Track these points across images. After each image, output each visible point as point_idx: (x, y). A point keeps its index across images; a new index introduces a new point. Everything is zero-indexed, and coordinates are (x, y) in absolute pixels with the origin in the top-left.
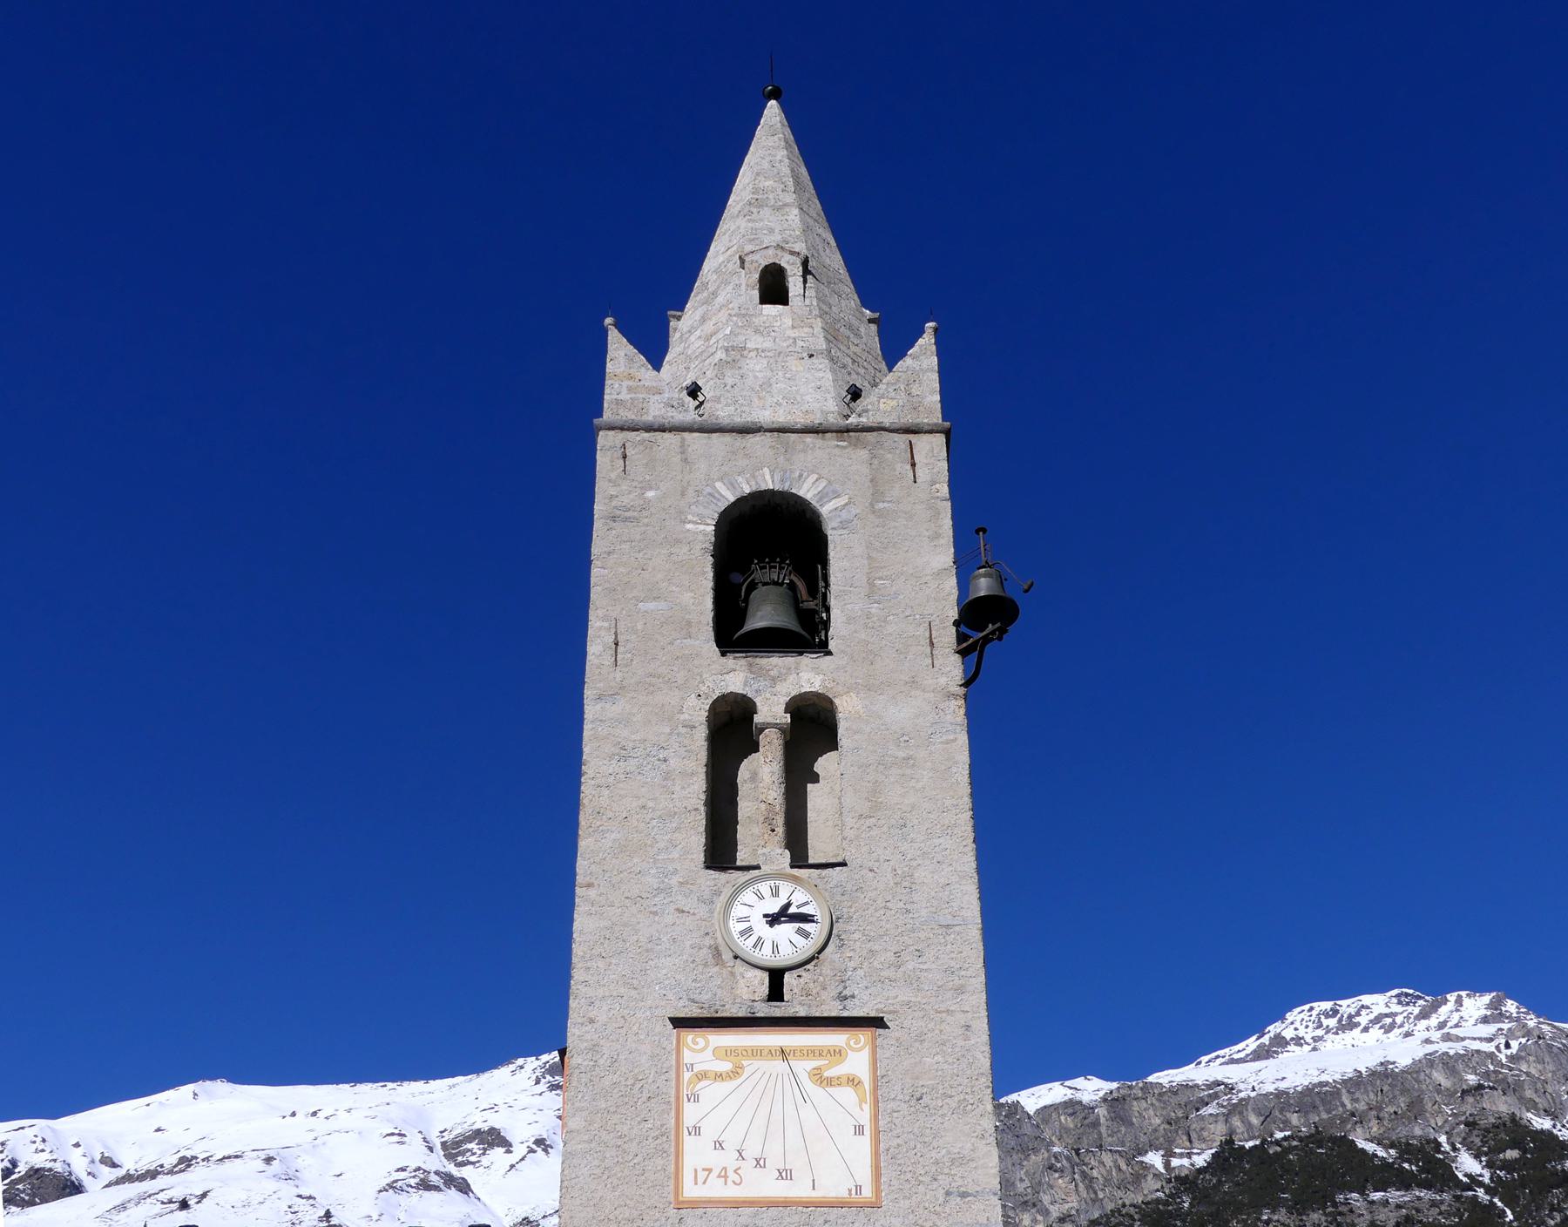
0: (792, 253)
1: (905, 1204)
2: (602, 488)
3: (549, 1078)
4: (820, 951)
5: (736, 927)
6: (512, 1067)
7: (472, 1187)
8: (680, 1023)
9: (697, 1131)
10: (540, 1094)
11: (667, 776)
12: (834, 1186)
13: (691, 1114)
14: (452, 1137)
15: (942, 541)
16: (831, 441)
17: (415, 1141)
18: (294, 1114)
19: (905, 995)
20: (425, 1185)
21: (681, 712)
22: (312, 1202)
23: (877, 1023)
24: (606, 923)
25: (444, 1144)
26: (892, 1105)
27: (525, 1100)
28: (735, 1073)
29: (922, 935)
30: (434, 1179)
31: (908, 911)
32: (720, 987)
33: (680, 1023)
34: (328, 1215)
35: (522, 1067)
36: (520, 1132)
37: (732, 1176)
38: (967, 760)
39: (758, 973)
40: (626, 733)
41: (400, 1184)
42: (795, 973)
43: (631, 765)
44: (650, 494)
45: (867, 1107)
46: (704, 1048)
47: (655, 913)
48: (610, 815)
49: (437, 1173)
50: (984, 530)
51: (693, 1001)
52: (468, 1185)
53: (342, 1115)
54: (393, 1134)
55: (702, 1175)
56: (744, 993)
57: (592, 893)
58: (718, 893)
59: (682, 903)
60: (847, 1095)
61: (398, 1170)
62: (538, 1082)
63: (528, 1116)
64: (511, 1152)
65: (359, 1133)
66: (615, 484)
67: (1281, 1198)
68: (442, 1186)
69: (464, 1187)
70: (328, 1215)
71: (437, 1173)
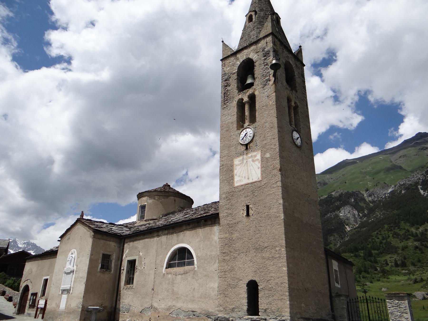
9: (236, 175)
12: (255, 179)
13: (235, 172)
45: (260, 164)
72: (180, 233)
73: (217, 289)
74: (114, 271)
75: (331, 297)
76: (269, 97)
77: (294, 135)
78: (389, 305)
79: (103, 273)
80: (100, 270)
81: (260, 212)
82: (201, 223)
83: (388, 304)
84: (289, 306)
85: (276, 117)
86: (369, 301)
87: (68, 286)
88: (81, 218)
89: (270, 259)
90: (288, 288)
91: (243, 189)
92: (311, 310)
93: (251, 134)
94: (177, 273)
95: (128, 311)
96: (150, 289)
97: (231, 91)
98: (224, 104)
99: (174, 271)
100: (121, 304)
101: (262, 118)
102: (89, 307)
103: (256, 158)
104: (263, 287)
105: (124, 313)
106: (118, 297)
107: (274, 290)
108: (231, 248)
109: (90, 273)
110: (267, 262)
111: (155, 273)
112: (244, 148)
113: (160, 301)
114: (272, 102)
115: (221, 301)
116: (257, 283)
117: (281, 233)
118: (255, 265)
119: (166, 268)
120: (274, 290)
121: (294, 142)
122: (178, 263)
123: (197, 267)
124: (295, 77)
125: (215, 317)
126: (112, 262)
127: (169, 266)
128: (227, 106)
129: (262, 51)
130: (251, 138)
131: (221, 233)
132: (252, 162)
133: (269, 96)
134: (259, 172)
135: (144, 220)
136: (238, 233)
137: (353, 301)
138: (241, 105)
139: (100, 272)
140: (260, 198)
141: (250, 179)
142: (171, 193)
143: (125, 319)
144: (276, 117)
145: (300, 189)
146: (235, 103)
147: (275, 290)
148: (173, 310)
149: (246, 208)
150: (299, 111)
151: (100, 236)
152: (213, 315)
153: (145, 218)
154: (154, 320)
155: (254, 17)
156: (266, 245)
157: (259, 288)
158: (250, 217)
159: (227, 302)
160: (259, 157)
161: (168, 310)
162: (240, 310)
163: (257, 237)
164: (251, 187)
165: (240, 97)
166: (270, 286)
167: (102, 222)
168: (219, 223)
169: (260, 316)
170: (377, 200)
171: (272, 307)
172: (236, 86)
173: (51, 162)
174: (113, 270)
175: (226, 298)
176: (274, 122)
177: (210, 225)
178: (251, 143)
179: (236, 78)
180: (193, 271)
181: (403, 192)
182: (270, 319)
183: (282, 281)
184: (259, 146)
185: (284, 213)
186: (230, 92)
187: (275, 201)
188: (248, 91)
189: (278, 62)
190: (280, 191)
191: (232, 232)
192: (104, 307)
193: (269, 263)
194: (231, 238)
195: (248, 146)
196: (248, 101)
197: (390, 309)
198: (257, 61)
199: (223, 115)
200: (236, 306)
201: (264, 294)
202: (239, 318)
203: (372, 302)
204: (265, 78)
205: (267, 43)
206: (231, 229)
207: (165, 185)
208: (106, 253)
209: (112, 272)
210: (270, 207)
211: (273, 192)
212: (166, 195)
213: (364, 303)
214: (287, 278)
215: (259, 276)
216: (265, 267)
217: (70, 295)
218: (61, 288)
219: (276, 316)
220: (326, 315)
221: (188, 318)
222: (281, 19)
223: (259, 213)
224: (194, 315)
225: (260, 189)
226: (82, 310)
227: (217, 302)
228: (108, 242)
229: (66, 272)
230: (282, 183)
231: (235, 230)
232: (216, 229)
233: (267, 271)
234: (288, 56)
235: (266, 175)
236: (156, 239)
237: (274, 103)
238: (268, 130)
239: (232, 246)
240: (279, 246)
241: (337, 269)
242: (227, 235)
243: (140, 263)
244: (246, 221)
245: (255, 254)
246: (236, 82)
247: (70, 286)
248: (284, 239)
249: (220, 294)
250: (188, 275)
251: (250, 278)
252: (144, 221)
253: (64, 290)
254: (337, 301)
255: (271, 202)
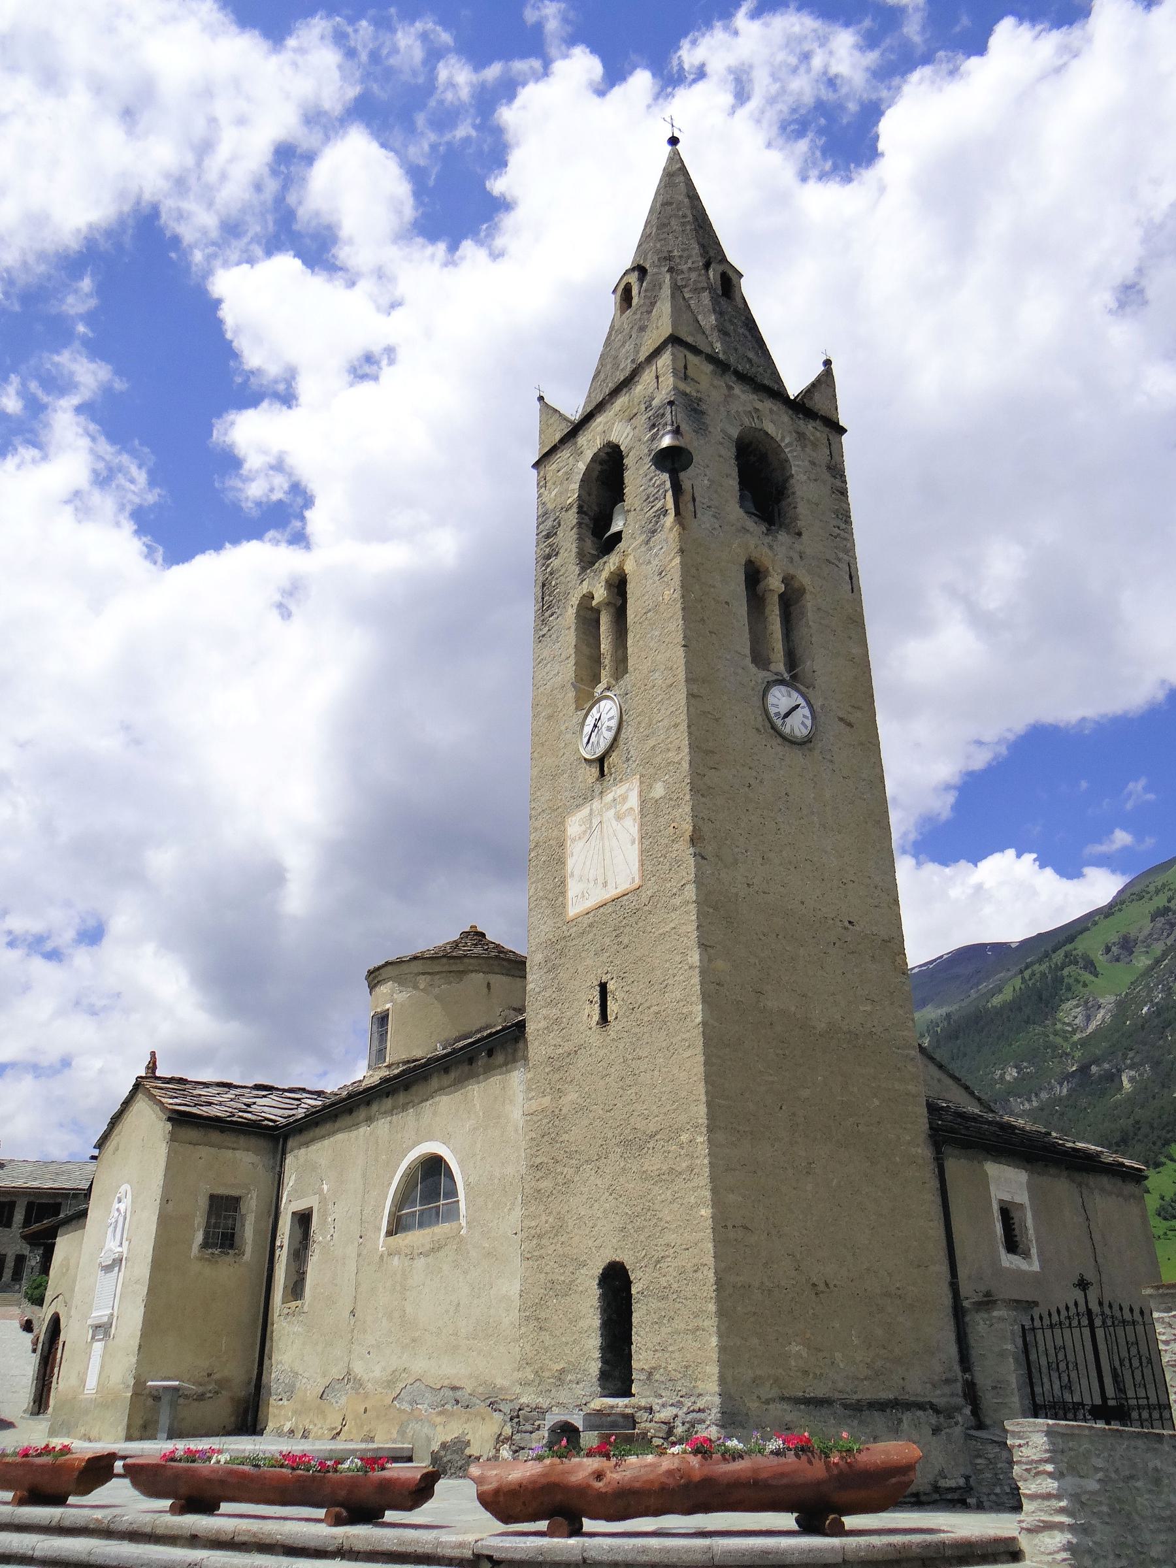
9: (572, 875)
12: (624, 886)
13: (570, 863)
72: (424, 1104)
73: (517, 1303)
74: (253, 1252)
75: (958, 1313)
76: (663, 574)
77: (771, 699)
78: (1163, 1331)
79: (210, 1261)
80: (199, 1252)
81: (637, 1006)
82: (480, 1063)
83: (1159, 1328)
84: (715, 1356)
85: (684, 646)
86: (1098, 1322)
87: (106, 1313)
88: (149, 1075)
89: (664, 1177)
90: (715, 1287)
91: (591, 925)
92: (842, 1365)
93: (612, 718)
94: (416, 1252)
95: (291, 1391)
96: (347, 1313)
97: (561, 573)
98: (543, 621)
99: (406, 1242)
100: (274, 1369)
101: (643, 655)
102: (150, 1383)
103: (626, 807)
104: (645, 1287)
105: (281, 1400)
106: (267, 1344)
107: (675, 1296)
108: (558, 1145)
109: (159, 1264)
110: (656, 1190)
111: (359, 1255)
112: (595, 771)
113: (369, 1353)
114: (672, 591)
115: (528, 1347)
116: (626, 1271)
117: (695, 1079)
118: (622, 1203)
119: (390, 1233)
120: (675, 1296)
121: (773, 727)
122: (422, 1212)
123: (467, 1223)
124: (793, 481)
125: (511, 1405)
126: (247, 1222)
127: (397, 1226)
128: (549, 630)
129: (646, 408)
130: (613, 732)
131: (530, 1096)
132: (614, 823)
133: (662, 571)
134: (633, 854)
135: (386, 1067)
136: (577, 1088)
137: (1042, 1325)
138: (588, 617)
139: (201, 1259)
140: (638, 954)
141: (609, 886)
142: (472, 961)
143: (282, 1423)
144: (683, 643)
145: (803, 903)
146: (570, 614)
147: (678, 1297)
148: (402, 1385)
149: (598, 996)
150: (809, 605)
151: (192, 1134)
152: (507, 1400)
153: (387, 1060)
154: (353, 1422)
155: (635, 292)
156: (652, 1128)
157: (634, 1291)
158: (608, 1028)
159: (546, 1349)
160: (633, 801)
161: (390, 1384)
162: (579, 1376)
163: (629, 1100)
164: (613, 915)
165: (585, 588)
167: (227, 1083)
168: (526, 1058)
169: (634, 1395)
172: (575, 550)
173: (275, 876)
174: (248, 1249)
175: (545, 1336)
176: (675, 666)
177: (500, 1066)
178: (613, 751)
179: (575, 521)
180: (456, 1242)
182: (663, 1406)
183: (694, 1261)
184: (635, 761)
185: (704, 1001)
186: (557, 575)
187: (678, 958)
188: (605, 562)
189: (676, 443)
190: (692, 921)
191: (560, 1087)
192: (217, 1382)
193: (660, 1195)
194: (557, 1112)
195: (606, 765)
196: (606, 601)
197: (1167, 1348)
198: (630, 450)
199: (540, 663)
200: (569, 1363)
201: (645, 1312)
202: (577, 1406)
204: (652, 507)
205: (657, 377)
206: (557, 1076)
207: (466, 932)
208: (221, 1191)
209: (247, 1256)
210: (666, 982)
211: (672, 925)
212: (454, 968)
213: (1043, 1329)
214: (710, 1246)
215: (632, 1246)
216: (649, 1210)
217: (110, 1342)
218: (90, 1322)
219: (681, 1394)
220: (928, 1386)
221: (440, 1413)
222: (741, 276)
223: (633, 1009)
224: (457, 1402)
225: (635, 918)
226: (136, 1394)
227: (518, 1349)
228: (229, 1154)
229: (103, 1264)
230: (697, 888)
231: (569, 1079)
232: (517, 1078)
233: (655, 1225)
234: (757, 410)
235: (654, 865)
236: (364, 1130)
237: (677, 595)
238: (659, 699)
239: (561, 1139)
240: (689, 1127)
242: (546, 1101)
243: (324, 1215)
244: (598, 1043)
245: (622, 1164)
246: (576, 536)
247: (109, 1312)
248: (703, 1098)
249: (527, 1318)
250: (441, 1254)
251: (608, 1255)
252: (385, 1069)
253: (96, 1327)
254: (979, 1324)
255: (668, 965)
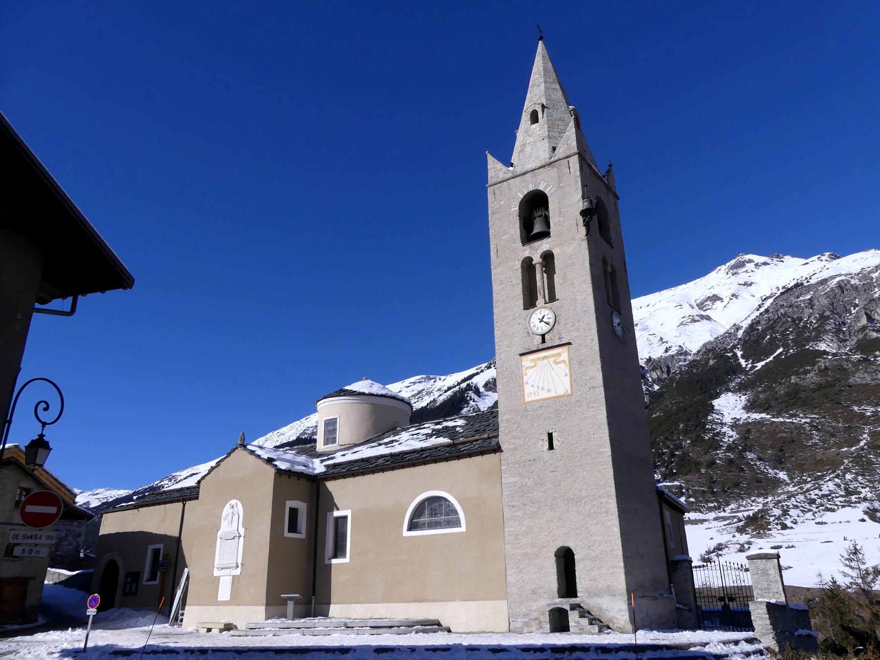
0: (538, 104)
1: (579, 393)
2: (490, 205)
3: (731, 271)
4: (553, 327)
5: (532, 325)
6: (716, 271)
7: (711, 317)
8: (521, 355)
9: (527, 383)
10: (729, 278)
11: (513, 286)
12: (561, 392)
13: (525, 379)
14: (700, 301)
15: (578, 191)
16: (547, 168)
17: (687, 307)
18: (641, 307)
19: (575, 334)
20: (694, 321)
21: (514, 266)
22: (654, 335)
23: (569, 344)
24: (502, 332)
25: (697, 305)
26: (574, 366)
27: (724, 281)
28: (535, 366)
29: (579, 315)
30: (697, 318)
31: (575, 309)
32: (530, 343)
33: (521, 355)
34: (661, 339)
35: (720, 270)
36: (725, 294)
37: (537, 394)
38: (589, 259)
39: (539, 336)
40: (501, 277)
41: (684, 323)
42: (548, 334)
43: (503, 286)
44: (502, 203)
45: (567, 368)
46: (527, 360)
47: (513, 326)
48: (500, 301)
49: (697, 316)
50: (586, 186)
51: (524, 348)
52: (710, 317)
53: (658, 303)
54: (677, 306)
55: (529, 394)
56: (536, 343)
57: (498, 324)
58: (527, 316)
59: (519, 321)
60: (562, 365)
61: (682, 318)
62: (727, 273)
63: (726, 287)
64: (723, 301)
65: (666, 308)
66: (492, 203)
67: (767, 343)
68: (700, 320)
69: (708, 318)
70: (661, 339)
71: (697, 316)
91: (541, 407)
93: (550, 318)
138: (528, 266)
156: (584, 494)
165: (527, 254)
166: (593, 554)
170: (665, 378)
171: (598, 584)
181: (711, 362)
203: (729, 568)
239: (527, 495)
241: (670, 523)
251: (560, 544)
